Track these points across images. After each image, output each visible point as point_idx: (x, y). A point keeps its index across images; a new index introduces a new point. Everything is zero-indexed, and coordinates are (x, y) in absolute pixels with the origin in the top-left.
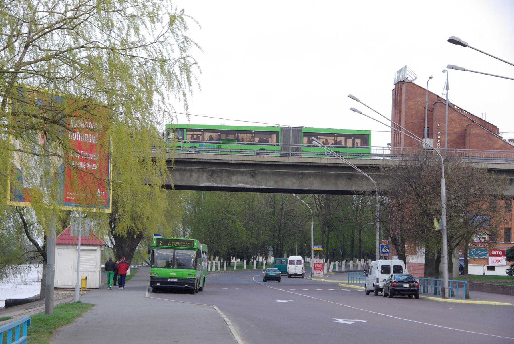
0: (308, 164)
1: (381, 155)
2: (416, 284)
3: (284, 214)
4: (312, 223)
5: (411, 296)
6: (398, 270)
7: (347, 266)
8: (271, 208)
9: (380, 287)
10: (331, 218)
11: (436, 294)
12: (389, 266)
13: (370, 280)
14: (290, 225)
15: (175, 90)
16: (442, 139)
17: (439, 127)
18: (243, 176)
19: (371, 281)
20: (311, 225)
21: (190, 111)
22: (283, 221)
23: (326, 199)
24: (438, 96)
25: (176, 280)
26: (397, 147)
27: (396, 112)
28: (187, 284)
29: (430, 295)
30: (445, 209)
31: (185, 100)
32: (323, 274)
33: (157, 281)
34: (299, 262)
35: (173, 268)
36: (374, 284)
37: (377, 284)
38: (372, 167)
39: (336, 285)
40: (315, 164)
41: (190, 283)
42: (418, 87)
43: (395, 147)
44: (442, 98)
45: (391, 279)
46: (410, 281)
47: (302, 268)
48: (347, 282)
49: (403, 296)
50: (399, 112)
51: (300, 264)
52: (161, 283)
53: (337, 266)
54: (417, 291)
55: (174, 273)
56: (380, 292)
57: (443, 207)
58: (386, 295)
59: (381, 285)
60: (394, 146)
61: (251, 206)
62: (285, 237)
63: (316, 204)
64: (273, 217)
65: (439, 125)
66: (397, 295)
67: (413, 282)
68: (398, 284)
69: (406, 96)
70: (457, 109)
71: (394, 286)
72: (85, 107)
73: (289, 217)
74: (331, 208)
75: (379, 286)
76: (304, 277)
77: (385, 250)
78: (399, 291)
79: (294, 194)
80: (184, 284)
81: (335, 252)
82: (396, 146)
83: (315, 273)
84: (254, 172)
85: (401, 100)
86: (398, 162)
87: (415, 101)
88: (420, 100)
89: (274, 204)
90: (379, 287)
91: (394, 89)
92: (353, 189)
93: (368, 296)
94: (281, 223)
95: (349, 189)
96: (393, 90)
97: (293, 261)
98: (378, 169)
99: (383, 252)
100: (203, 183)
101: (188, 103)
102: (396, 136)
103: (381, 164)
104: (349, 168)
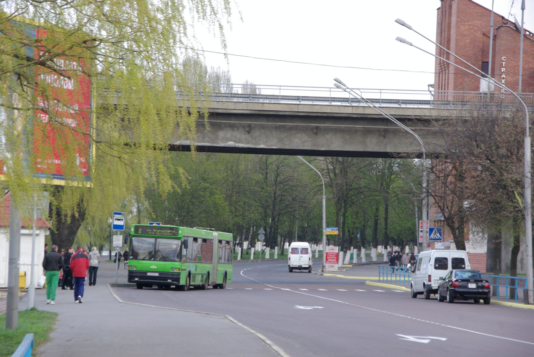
0: (325, 115)
1: (428, 102)
2: (487, 284)
3: (280, 183)
4: (324, 196)
5: (478, 300)
6: (458, 263)
7: (368, 256)
8: (262, 174)
9: (434, 288)
10: (348, 190)
11: (513, 297)
12: (446, 259)
13: (418, 278)
14: (288, 198)
15: (208, 21)
16: (508, 79)
17: (503, 61)
18: (234, 131)
19: (420, 279)
20: (322, 199)
21: (229, 50)
22: (278, 192)
23: (342, 163)
24: (503, 18)
25: (157, 275)
26: (443, 91)
27: (443, 40)
28: (170, 278)
29: (504, 299)
30: (529, 179)
31: (222, 35)
32: (339, 267)
33: (134, 275)
34: (305, 251)
35: (154, 260)
36: (424, 283)
37: (429, 283)
38: (418, 120)
39: (362, 284)
40: (335, 115)
41: (173, 278)
42: (474, 4)
43: (440, 91)
44: (509, 21)
45: (450, 277)
46: (476, 278)
47: (310, 259)
48: (377, 278)
49: (465, 300)
50: (446, 40)
51: (307, 253)
52: (140, 278)
53: (355, 256)
54: (487, 294)
55: (155, 266)
56: (432, 296)
57: (527, 177)
58: (443, 299)
59: (435, 286)
60: (439, 90)
61: (234, 172)
62: (281, 215)
63: (328, 169)
64: (265, 187)
65: (504, 58)
66: (459, 299)
67: (482, 281)
68: (461, 284)
69: (458, 17)
70: (529, 35)
71: (455, 286)
72: (85, 42)
73: (287, 187)
74: (349, 175)
75: (432, 285)
76: (312, 272)
77: (435, 236)
78: (462, 293)
79: (300, 157)
80: (166, 279)
81: (352, 236)
82: (445, 90)
83: (327, 265)
84: (249, 126)
85: (450, 23)
86: (455, 112)
87: (470, 25)
88: (477, 24)
89: (267, 169)
90: (432, 287)
91: (439, 8)
92: (388, 150)
93: (414, 299)
94: (276, 195)
95: (382, 150)
96: (437, 9)
97: (296, 249)
98: (428, 123)
99: (433, 238)
100: (177, 140)
101: (226, 39)
102: (442, 74)
103: (433, 115)
104: (385, 120)
